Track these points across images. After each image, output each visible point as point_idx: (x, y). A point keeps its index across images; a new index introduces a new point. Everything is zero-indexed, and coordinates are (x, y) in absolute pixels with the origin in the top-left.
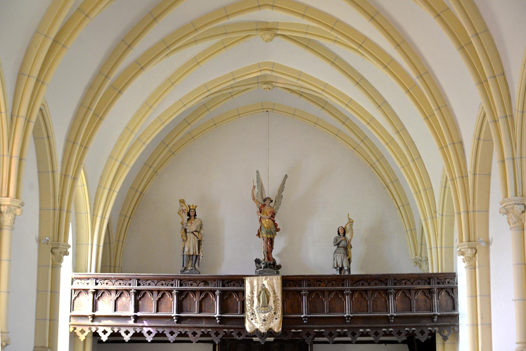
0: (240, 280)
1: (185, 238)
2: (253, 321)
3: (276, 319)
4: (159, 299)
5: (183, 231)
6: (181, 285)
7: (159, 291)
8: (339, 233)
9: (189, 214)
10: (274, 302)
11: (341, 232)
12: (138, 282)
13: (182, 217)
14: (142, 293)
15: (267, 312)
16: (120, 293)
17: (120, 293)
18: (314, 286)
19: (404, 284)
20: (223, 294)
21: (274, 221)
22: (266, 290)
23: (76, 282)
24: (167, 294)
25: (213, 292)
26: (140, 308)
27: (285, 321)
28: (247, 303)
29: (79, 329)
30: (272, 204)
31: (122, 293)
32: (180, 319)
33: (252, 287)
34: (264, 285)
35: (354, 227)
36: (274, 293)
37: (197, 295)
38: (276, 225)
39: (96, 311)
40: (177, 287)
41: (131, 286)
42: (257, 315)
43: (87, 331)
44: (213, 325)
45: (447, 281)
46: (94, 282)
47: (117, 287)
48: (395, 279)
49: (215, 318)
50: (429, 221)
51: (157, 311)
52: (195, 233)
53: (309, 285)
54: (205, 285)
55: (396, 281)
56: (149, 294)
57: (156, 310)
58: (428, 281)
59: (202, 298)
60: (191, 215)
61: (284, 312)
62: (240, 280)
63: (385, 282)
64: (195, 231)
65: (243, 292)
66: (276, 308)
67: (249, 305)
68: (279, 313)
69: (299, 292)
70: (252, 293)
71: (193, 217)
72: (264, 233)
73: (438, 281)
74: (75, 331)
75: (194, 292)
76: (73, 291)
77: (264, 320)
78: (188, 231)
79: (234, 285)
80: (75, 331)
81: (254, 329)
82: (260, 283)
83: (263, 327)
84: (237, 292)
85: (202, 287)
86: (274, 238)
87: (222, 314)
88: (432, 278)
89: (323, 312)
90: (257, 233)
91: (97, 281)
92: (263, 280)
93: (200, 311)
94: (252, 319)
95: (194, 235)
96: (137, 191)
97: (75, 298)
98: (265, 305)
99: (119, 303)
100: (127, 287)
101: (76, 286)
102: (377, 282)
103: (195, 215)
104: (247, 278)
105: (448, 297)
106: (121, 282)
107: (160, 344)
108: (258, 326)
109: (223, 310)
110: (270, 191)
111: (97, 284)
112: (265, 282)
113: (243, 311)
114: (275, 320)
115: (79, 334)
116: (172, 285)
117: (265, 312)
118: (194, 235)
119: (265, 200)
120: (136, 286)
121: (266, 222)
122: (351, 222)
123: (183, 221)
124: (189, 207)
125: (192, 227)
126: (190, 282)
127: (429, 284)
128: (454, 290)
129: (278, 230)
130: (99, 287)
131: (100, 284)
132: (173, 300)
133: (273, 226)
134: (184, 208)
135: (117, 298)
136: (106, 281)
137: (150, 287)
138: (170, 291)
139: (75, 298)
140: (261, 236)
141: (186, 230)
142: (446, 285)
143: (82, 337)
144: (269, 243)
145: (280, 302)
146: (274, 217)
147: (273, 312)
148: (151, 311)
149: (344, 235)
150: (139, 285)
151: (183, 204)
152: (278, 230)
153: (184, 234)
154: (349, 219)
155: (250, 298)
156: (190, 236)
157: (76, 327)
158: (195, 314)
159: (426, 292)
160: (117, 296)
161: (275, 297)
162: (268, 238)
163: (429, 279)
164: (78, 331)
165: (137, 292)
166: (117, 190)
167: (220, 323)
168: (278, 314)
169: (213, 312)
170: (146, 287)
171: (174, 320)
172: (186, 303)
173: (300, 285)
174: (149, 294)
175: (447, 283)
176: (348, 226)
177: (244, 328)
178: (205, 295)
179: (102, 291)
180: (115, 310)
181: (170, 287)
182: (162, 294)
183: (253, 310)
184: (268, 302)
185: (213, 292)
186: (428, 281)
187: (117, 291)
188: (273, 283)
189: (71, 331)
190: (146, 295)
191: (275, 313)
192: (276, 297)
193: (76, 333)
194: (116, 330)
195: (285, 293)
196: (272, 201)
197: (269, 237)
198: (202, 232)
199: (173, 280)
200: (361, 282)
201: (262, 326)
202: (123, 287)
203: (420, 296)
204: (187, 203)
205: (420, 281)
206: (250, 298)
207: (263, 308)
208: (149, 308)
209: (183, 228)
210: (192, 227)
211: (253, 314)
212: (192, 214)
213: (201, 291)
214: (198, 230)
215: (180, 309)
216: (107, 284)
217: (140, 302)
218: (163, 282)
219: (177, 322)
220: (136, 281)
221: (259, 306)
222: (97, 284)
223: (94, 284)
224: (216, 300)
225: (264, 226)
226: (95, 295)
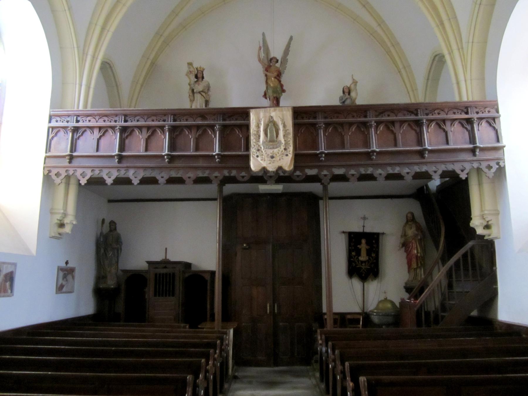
0: (243, 113)
1: (192, 98)
2: (259, 159)
3: (287, 155)
4: (149, 137)
5: (190, 91)
6: (175, 120)
7: (149, 128)
8: (344, 92)
9: (196, 77)
10: (284, 136)
11: (346, 91)
12: (125, 118)
13: (189, 78)
14: (129, 130)
15: (276, 148)
16: (103, 130)
17: (103, 130)
18: (331, 118)
19: (437, 114)
20: (224, 128)
21: (280, 81)
22: (275, 124)
23: (54, 120)
24: (159, 131)
25: (212, 127)
26: (126, 148)
27: (297, 157)
28: (252, 139)
29: (54, 171)
30: (278, 65)
31: (106, 131)
32: (172, 158)
33: (257, 121)
34: (272, 117)
35: (358, 88)
36: (284, 126)
37: (193, 132)
38: (282, 86)
39: (75, 151)
40: (170, 122)
41: (117, 123)
42: (263, 151)
43: (64, 174)
44: (213, 165)
45: (487, 110)
46: (75, 119)
47: (101, 123)
48: (426, 109)
49: (214, 156)
50: (456, 53)
51: (146, 150)
52: (203, 94)
53: (326, 118)
54: (202, 120)
55: (427, 112)
56: (137, 132)
57: (144, 149)
58: (465, 110)
59: (199, 135)
60: (199, 76)
61: (295, 148)
62: (243, 113)
63: (415, 112)
64: (202, 91)
65: (248, 127)
66: (286, 143)
67: (254, 141)
68: (291, 149)
69: (314, 125)
70: (258, 126)
71: (201, 79)
72: (270, 93)
73: (477, 110)
74: (50, 174)
75: (189, 127)
76: (51, 130)
77: (272, 157)
78: (195, 91)
79: (236, 119)
80: (50, 174)
81: (260, 168)
82: (268, 115)
83: (270, 165)
84: (240, 127)
85: (200, 122)
86: (280, 97)
87: (222, 152)
88: (470, 107)
89: (343, 147)
90: (263, 94)
91: (79, 118)
92: (271, 112)
93: (197, 149)
94: (257, 156)
95: (202, 95)
96: (148, 59)
97: (53, 138)
98: (272, 142)
99: (103, 142)
100: (113, 124)
101: (54, 124)
102: (406, 112)
103: (203, 78)
104: (251, 110)
105: (490, 129)
106: (106, 118)
107: (169, 202)
108: (264, 164)
109: (224, 146)
110: (277, 52)
111: (78, 121)
112: (273, 114)
113: (247, 148)
114: (285, 157)
115: (54, 177)
116: (164, 121)
117: (273, 148)
118: (202, 95)
119: (271, 59)
120: (123, 123)
121: (273, 82)
122: (355, 83)
123: (190, 82)
124: (197, 69)
125: (199, 87)
126: (185, 118)
127: (467, 113)
128: (496, 120)
129: (284, 91)
130: (80, 124)
131: (81, 121)
132: (165, 137)
133: (279, 86)
134: (192, 69)
135: (101, 137)
136: (89, 118)
137: (139, 124)
138: (162, 128)
139: (53, 138)
140: (267, 96)
141: (193, 90)
142: (486, 115)
143: (58, 180)
144: (275, 102)
145: (291, 136)
146: (280, 77)
147: (282, 148)
148: (139, 151)
149: (349, 94)
150: (126, 121)
151: (191, 66)
152: (284, 91)
153: (191, 94)
154: (354, 80)
155: (255, 132)
156: (198, 96)
157: (51, 169)
158: (192, 153)
159: (464, 122)
160: (100, 135)
161: (285, 130)
162: (274, 97)
163: (467, 108)
164: (53, 174)
165: (124, 130)
166: (112, 29)
167: (219, 162)
168: (288, 150)
169: (213, 150)
170: (135, 123)
171: (165, 159)
172: (180, 141)
173: (315, 118)
174: (137, 132)
175: (487, 111)
176: (352, 86)
177: (249, 167)
178: (202, 131)
179: (83, 129)
180: (97, 150)
181: (161, 123)
182: (152, 131)
183: (259, 146)
184: (277, 136)
185: (212, 127)
186: (465, 110)
187: (100, 128)
188: (283, 117)
189: (46, 174)
190: (134, 133)
191: (285, 149)
192: (286, 131)
193: (50, 176)
194: (97, 172)
195: (296, 126)
196: (277, 61)
197: (275, 95)
198: (210, 93)
199: (165, 115)
200: (386, 113)
201: (270, 163)
202: (108, 124)
203: (457, 126)
204: (196, 65)
205: (455, 111)
206: (255, 132)
207: (271, 143)
208: (137, 146)
209: (191, 88)
210: (199, 87)
211: (258, 150)
212: (200, 75)
213: (198, 127)
214: (206, 91)
215: (172, 146)
216: (89, 121)
217: (127, 141)
218: (154, 118)
219: (169, 162)
220: (123, 117)
221: (267, 141)
222: (78, 121)
223: (75, 121)
224: (215, 136)
225: (270, 85)
226: (75, 134)
